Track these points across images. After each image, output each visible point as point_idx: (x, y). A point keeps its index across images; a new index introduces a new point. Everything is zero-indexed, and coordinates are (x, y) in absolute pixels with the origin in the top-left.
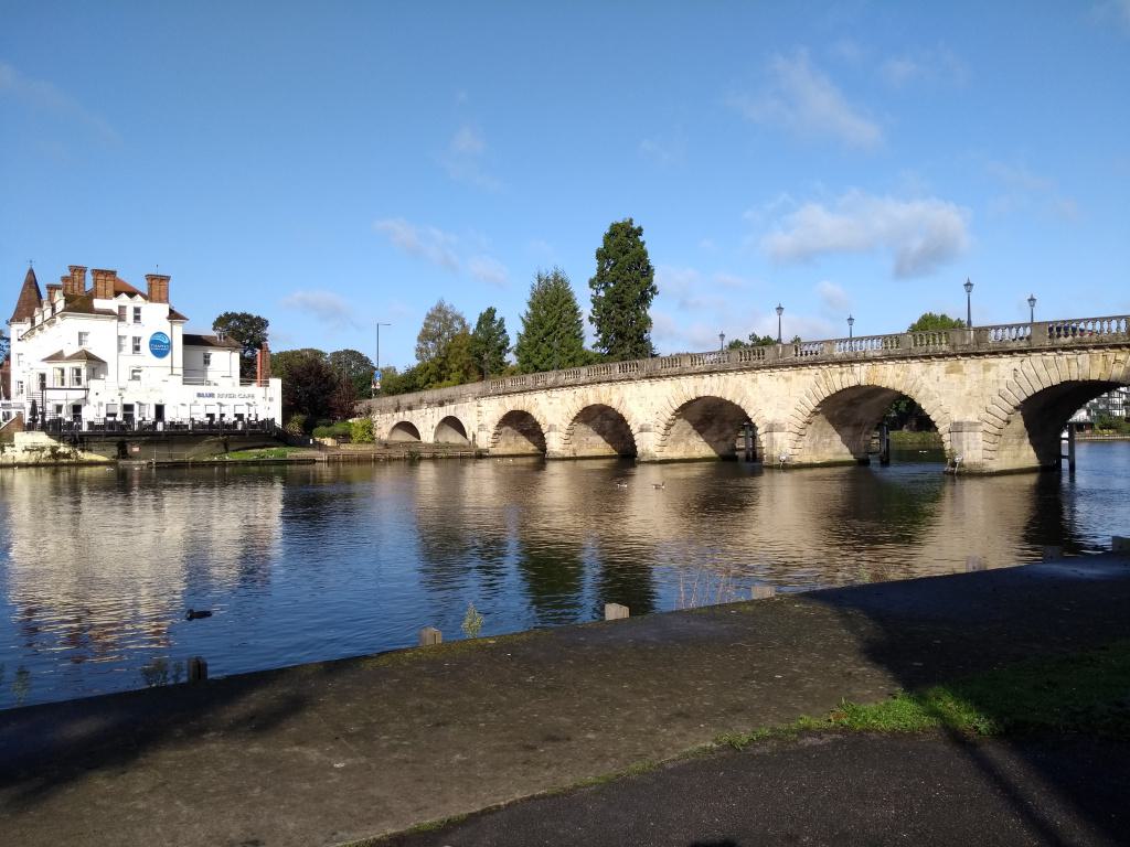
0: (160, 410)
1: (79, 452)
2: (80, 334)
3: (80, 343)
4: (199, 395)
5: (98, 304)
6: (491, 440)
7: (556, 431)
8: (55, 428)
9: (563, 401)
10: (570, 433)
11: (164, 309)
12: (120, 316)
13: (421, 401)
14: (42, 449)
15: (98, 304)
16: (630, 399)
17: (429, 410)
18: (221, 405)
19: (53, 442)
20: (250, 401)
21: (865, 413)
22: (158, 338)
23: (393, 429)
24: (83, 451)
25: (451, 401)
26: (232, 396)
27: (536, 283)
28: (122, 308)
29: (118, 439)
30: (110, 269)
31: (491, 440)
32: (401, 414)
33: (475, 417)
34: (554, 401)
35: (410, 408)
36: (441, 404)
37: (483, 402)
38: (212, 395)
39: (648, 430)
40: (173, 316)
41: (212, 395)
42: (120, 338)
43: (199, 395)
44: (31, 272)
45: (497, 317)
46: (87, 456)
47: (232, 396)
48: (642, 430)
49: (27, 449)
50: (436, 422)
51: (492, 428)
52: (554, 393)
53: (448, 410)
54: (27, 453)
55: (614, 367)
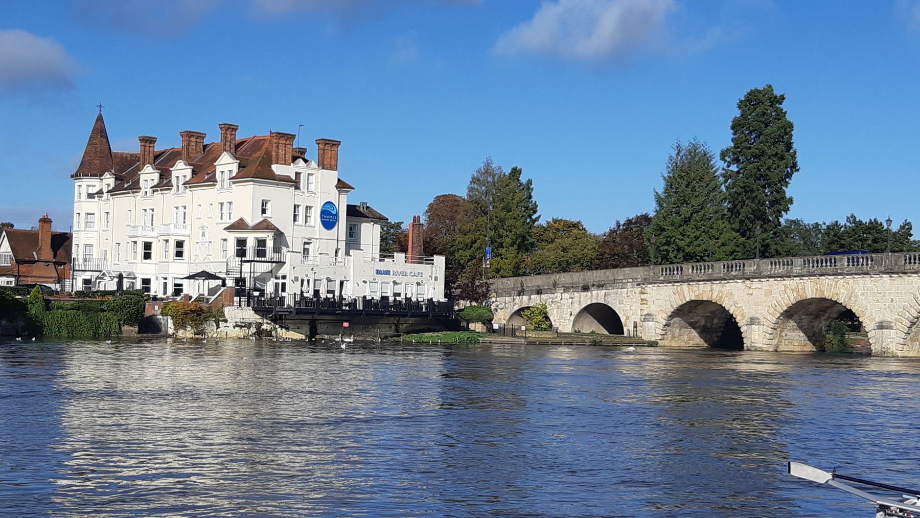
0: (146, 282)
1: (279, 330)
2: (307, 207)
3: (264, 211)
4: (378, 272)
5: (277, 169)
6: (660, 332)
7: (759, 324)
8: (263, 308)
9: (768, 293)
10: (778, 327)
11: (332, 177)
12: (294, 183)
13: (555, 285)
14: (249, 326)
15: (277, 169)
16: (863, 294)
17: (566, 295)
18: (395, 283)
19: (257, 318)
20: (419, 280)
21: (699, 317)
22: (328, 208)
23: (512, 316)
24: (281, 327)
25: (600, 286)
26: (404, 274)
27: (674, 155)
28: (298, 174)
29: (310, 317)
30: (291, 133)
31: (660, 332)
32: (525, 298)
33: (637, 306)
34: (755, 292)
35: (539, 292)
36: (586, 288)
37: (649, 288)
38: (388, 273)
39: (889, 327)
40: (342, 186)
41: (388, 273)
42: (296, 207)
43: (378, 272)
44: (100, 119)
45: (523, 179)
46: (282, 333)
47: (404, 274)
48: (881, 326)
49: (237, 326)
50: (577, 309)
51: (662, 319)
52: (756, 284)
53: (596, 296)
54: (237, 329)
55: (841, 260)
